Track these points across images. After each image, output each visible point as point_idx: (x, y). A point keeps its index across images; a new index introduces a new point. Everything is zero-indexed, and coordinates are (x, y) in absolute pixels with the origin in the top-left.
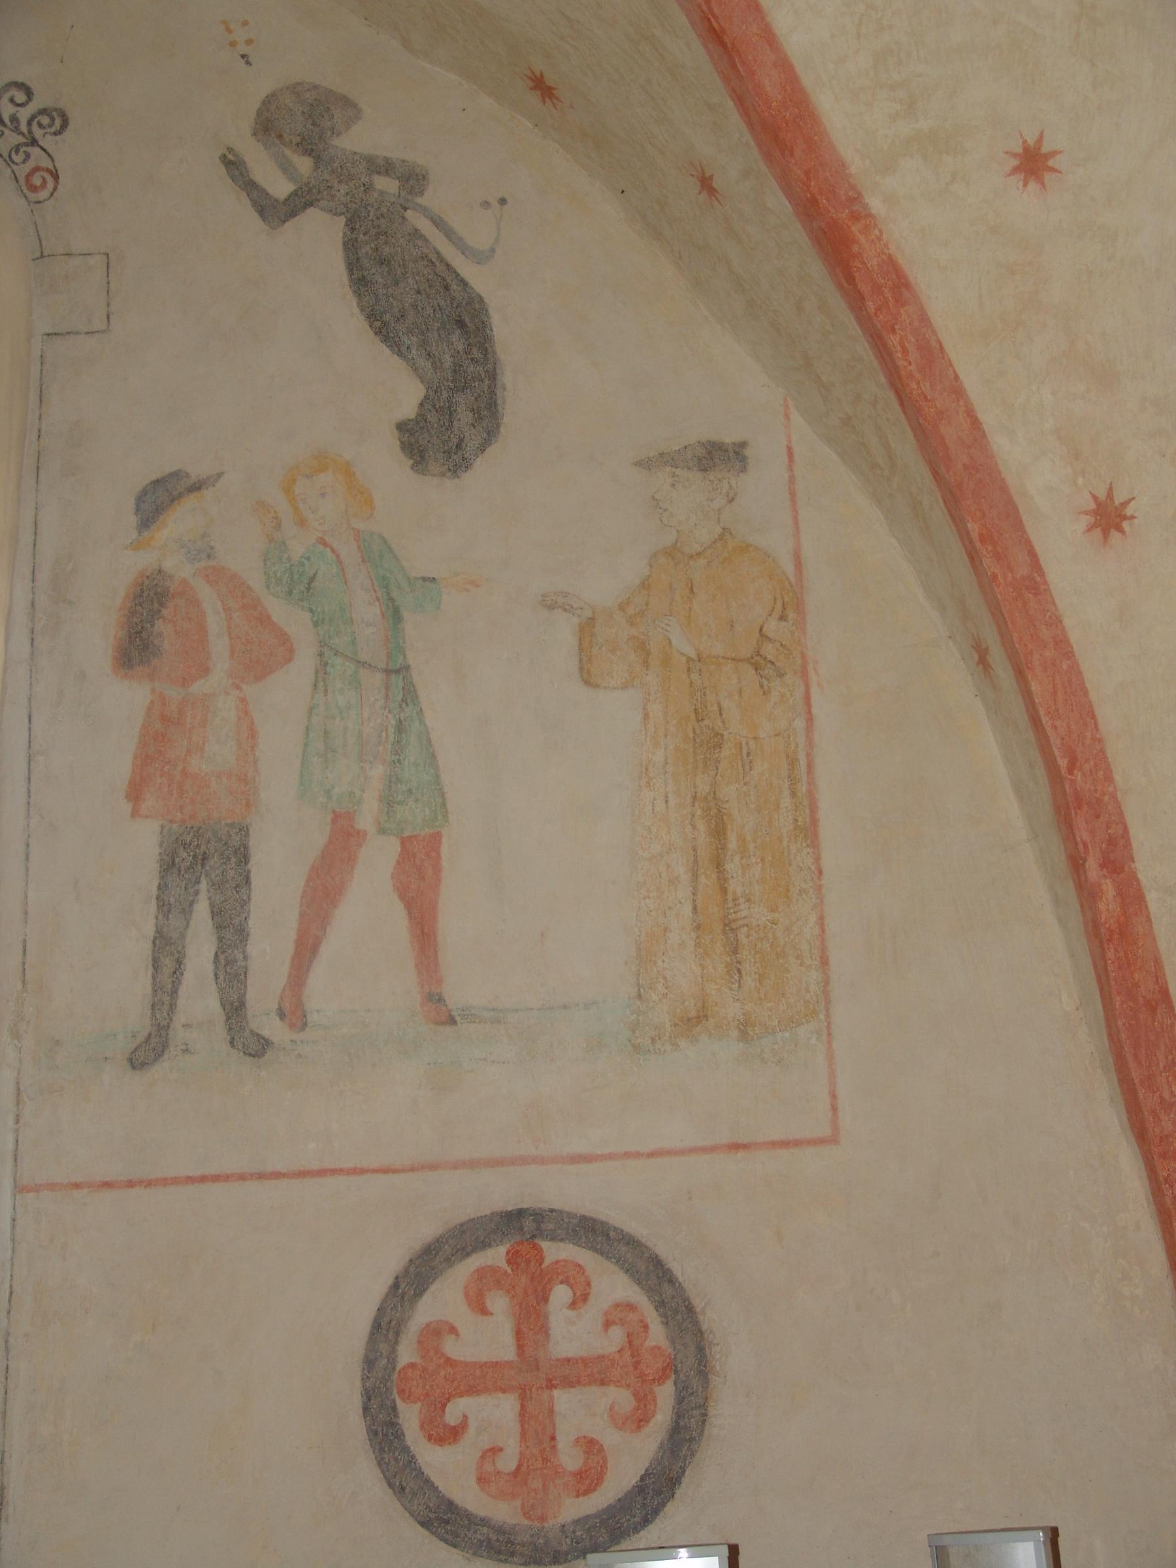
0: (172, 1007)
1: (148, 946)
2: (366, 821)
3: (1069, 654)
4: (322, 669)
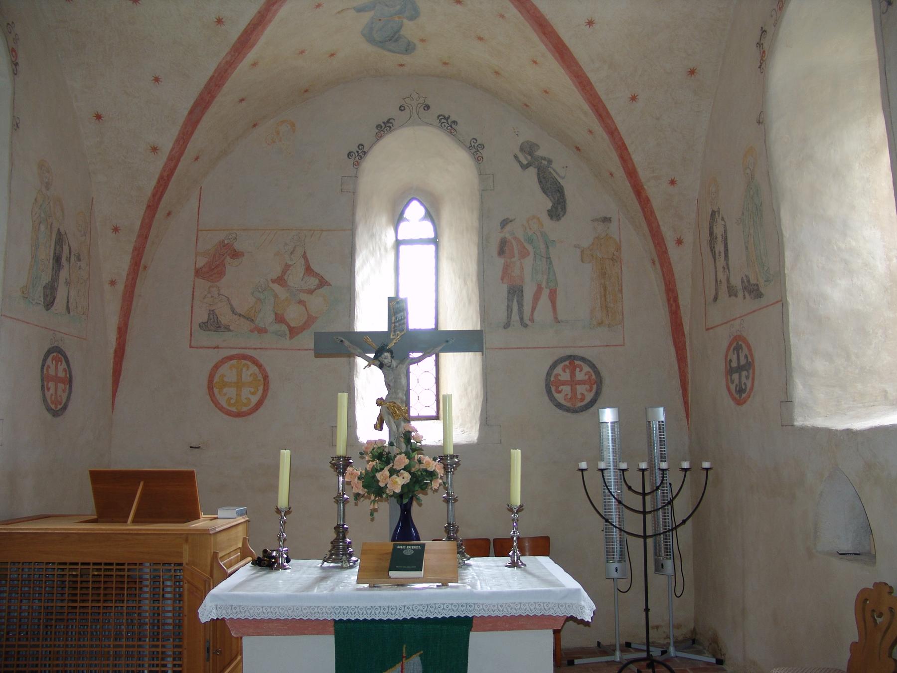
0: (511, 318)
1: (506, 307)
2: (543, 285)
3: (671, 264)
4: (535, 257)
